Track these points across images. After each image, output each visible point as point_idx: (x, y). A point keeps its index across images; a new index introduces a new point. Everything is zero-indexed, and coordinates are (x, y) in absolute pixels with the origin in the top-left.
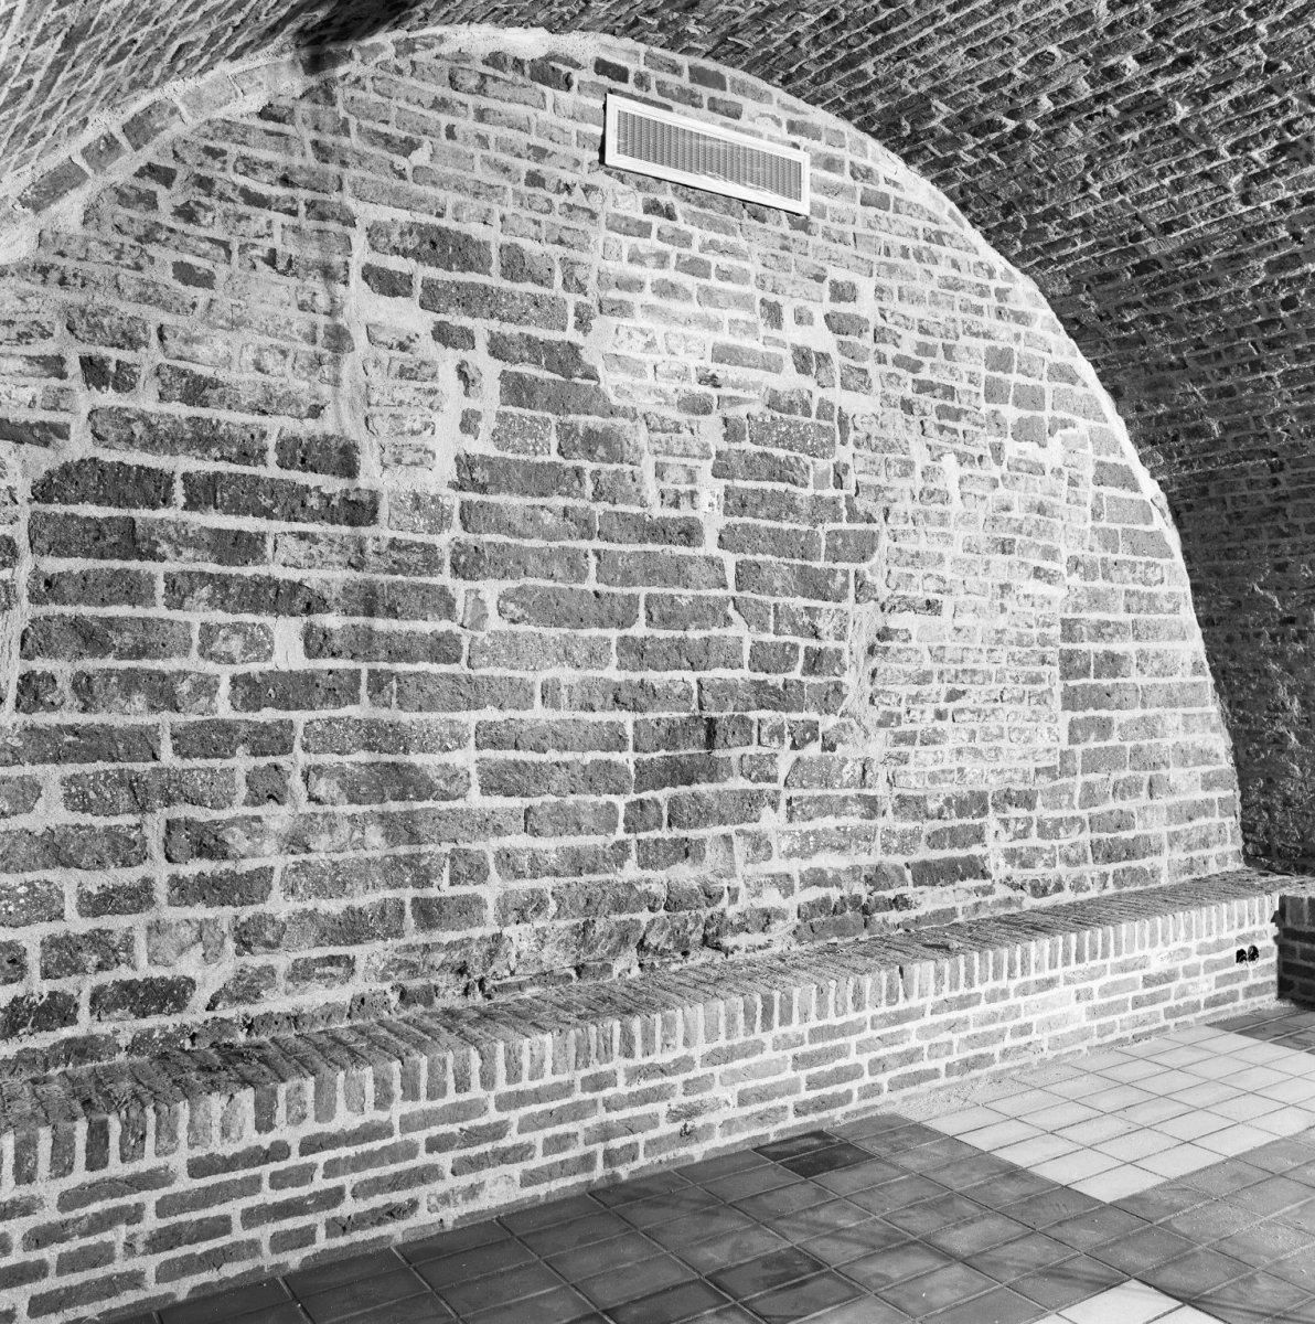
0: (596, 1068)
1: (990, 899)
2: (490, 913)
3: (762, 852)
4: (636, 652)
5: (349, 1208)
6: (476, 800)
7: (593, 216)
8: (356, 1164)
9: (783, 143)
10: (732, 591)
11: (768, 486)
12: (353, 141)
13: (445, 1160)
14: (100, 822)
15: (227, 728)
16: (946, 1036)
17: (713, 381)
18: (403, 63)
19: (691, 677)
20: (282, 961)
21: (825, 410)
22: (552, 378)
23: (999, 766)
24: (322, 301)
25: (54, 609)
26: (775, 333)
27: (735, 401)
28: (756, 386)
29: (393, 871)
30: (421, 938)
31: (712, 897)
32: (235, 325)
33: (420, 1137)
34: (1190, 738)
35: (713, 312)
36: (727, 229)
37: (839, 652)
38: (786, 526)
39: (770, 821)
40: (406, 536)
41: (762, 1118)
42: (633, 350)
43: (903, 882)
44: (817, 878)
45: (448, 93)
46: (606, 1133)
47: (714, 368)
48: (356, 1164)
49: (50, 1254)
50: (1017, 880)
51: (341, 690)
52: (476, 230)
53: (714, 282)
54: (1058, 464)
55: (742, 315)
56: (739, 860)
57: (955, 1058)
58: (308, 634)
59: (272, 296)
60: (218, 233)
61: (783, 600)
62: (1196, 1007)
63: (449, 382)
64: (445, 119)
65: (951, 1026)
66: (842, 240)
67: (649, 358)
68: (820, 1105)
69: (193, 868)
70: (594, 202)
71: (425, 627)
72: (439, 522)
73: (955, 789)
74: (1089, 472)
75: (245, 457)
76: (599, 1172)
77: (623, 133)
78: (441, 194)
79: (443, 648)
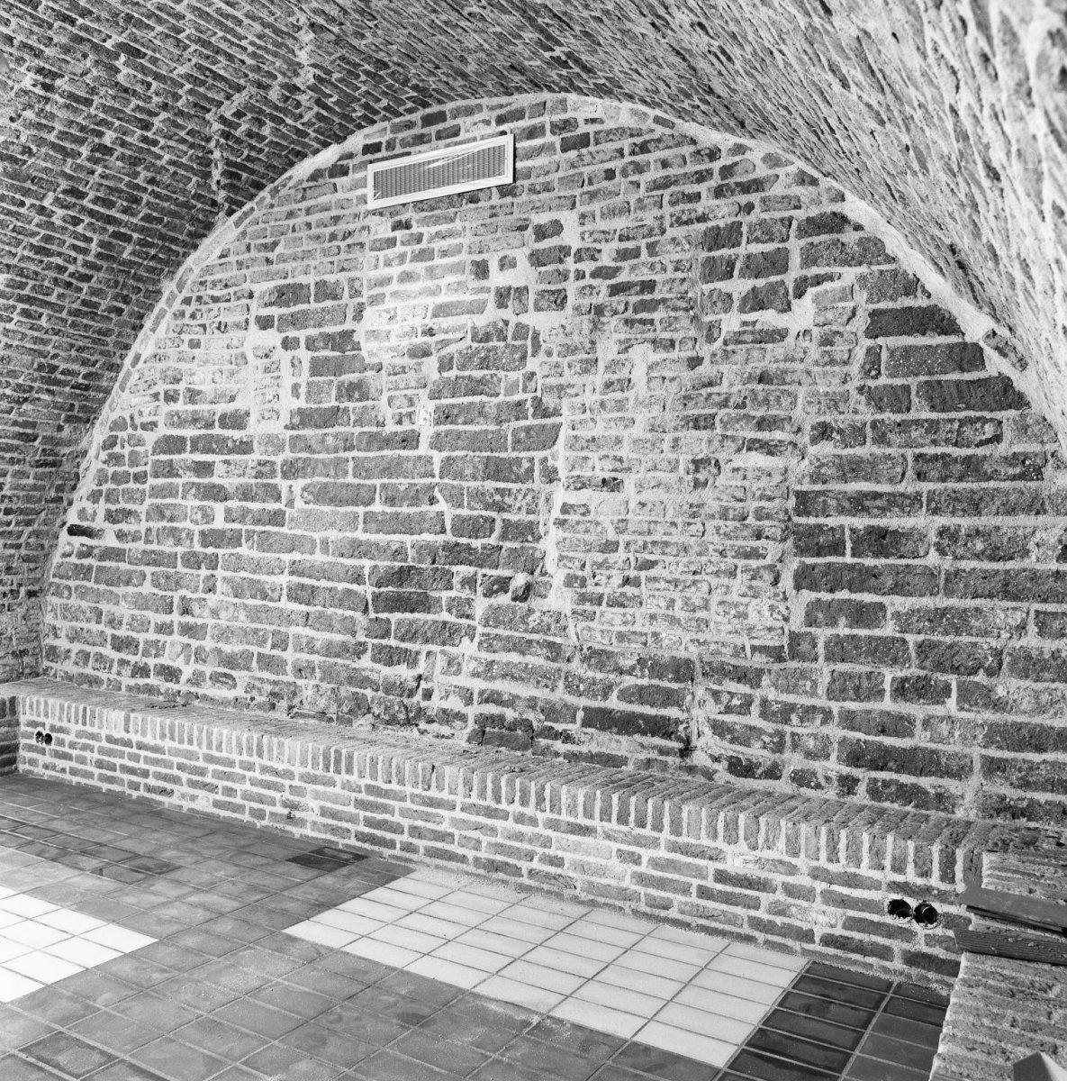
3: (454, 669)
9: (492, 136)
10: (437, 479)
17: (430, 332)
21: (521, 331)
23: (701, 637)
26: (485, 283)
41: (334, 830)
47: (430, 322)
56: (438, 669)
61: (473, 484)
62: (807, 936)
66: (548, 188)
74: (861, 322)
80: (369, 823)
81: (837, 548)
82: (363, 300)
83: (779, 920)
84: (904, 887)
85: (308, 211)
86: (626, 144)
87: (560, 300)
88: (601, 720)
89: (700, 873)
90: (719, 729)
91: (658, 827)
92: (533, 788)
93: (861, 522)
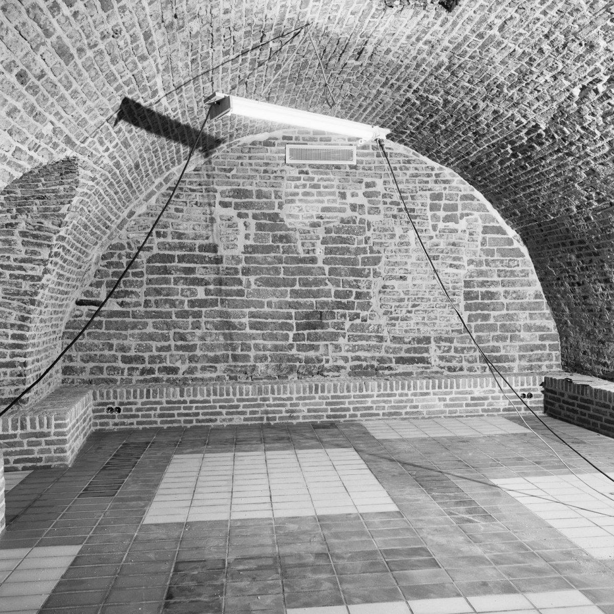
0: (263, 396)
1: (428, 371)
2: (252, 359)
4: (295, 293)
5: (201, 417)
6: (248, 330)
7: (283, 178)
8: (203, 408)
10: (327, 276)
11: (340, 246)
12: (216, 172)
13: (224, 411)
14: (160, 332)
15: (187, 312)
16: (383, 404)
17: (321, 218)
18: (229, 150)
19: (314, 300)
20: (199, 366)
22: (271, 222)
24: (208, 212)
25: (150, 286)
26: (344, 201)
27: (328, 222)
28: (336, 217)
29: (226, 347)
30: (233, 364)
31: (320, 361)
32: (188, 220)
33: (218, 405)
34: (533, 322)
35: (320, 198)
36: (326, 174)
37: (368, 293)
38: (346, 257)
39: (342, 341)
40: (230, 266)
41: (315, 417)
42: (295, 212)
43: (391, 362)
44: (358, 358)
45: (241, 154)
46: (267, 412)
47: (321, 214)
48: (203, 408)
49: (140, 413)
50: (442, 365)
51: (214, 303)
52: (249, 188)
53: (322, 189)
54: (464, 228)
55: (331, 198)
56: (330, 351)
57: (386, 411)
58: (206, 290)
59: (197, 212)
60: (184, 200)
61: (345, 278)
62: (498, 410)
63: (241, 226)
64: (240, 161)
65: (385, 402)
66: (370, 169)
67: (300, 214)
68: (335, 416)
69: (179, 343)
70: (283, 174)
71: (235, 288)
72: (239, 261)
73: (416, 335)
74: (480, 230)
75: (191, 250)
76: (265, 421)
77: (291, 154)
78: (239, 180)
79: (240, 293)
80: (332, 410)
81: (477, 298)
82: (283, 200)
83: (490, 408)
84: (524, 390)
85: (250, 158)
86: (401, 159)
87: (377, 211)
88: (400, 360)
89: (466, 399)
90: (441, 358)
91: (452, 388)
92: (406, 383)
93: (484, 290)
